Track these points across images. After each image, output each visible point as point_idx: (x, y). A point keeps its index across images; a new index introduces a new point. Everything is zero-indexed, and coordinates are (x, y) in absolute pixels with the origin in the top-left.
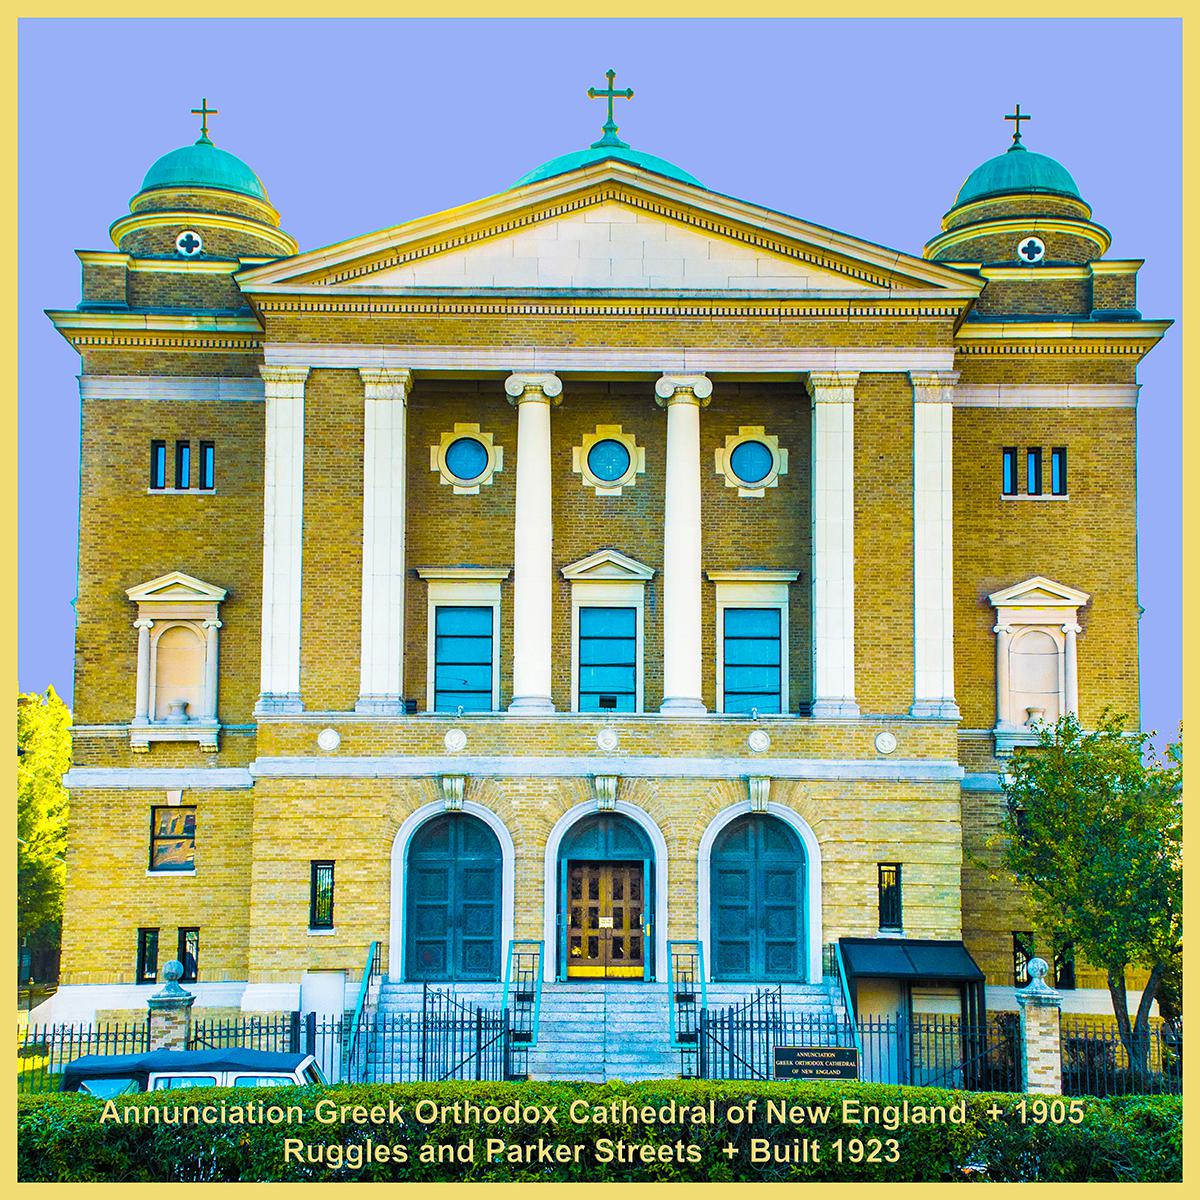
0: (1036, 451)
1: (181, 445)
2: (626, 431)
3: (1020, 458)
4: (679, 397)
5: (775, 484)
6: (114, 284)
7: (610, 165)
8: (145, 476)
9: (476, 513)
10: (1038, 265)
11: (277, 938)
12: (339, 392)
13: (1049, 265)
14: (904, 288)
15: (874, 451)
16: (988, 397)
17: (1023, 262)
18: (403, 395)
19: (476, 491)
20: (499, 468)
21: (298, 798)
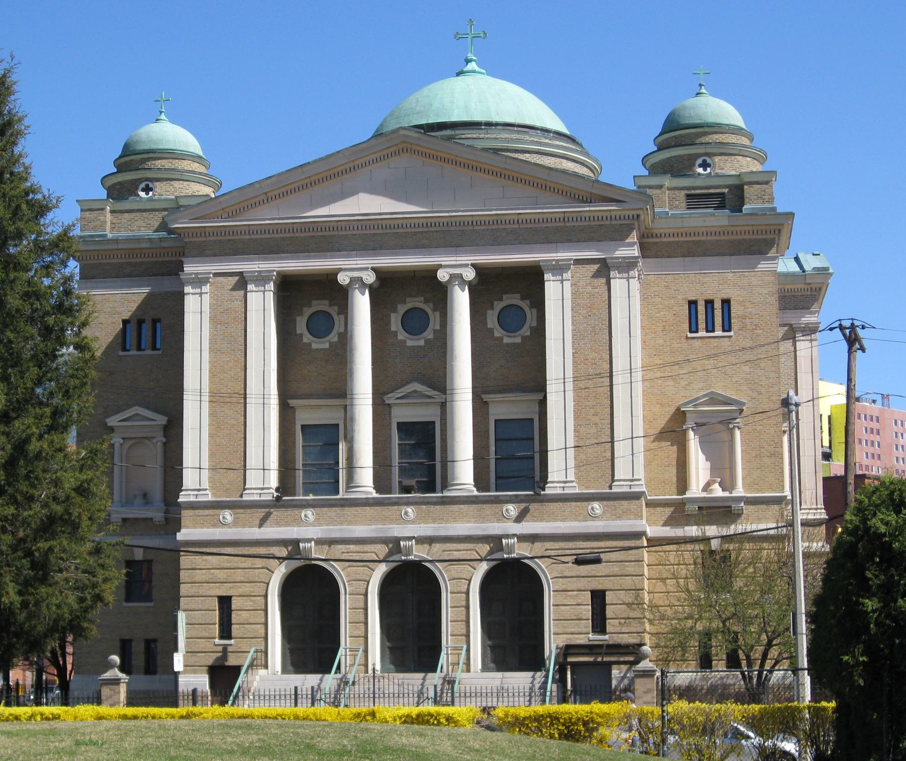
6: (99, 220)
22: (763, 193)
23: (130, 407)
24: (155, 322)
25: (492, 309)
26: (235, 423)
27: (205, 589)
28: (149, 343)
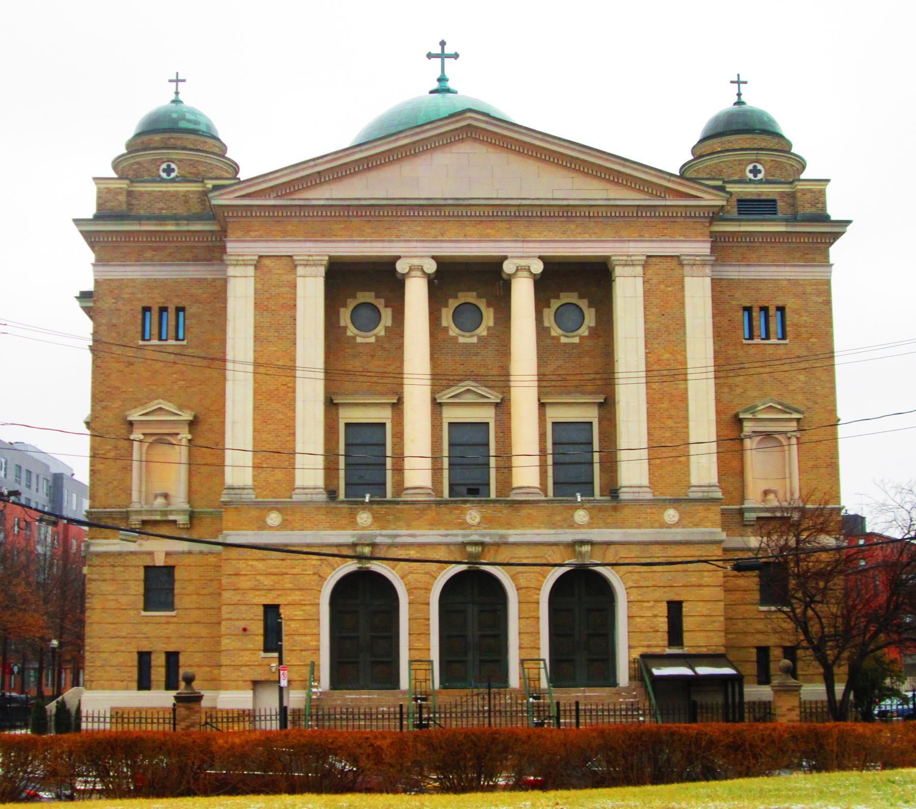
0: (765, 309)
1: (163, 310)
2: (377, 297)
3: (755, 314)
4: (413, 273)
5: (586, 334)
6: (117, 199)
7: (469, 115)
8: (137, 332)
9: (373, 356)
10: (760, 182)
11: (241, 659)
12: (279, 272)
13: (768, 182)
14: (671, 198)
15: (658, 310)
16: (732, 272)
17: (750, 180)
18: (323, 274)
19: (373, 340)
20: (389, 323)
21: (252, 560)
22: (816, 201)
25: (549, 307)
28: (172, 333)
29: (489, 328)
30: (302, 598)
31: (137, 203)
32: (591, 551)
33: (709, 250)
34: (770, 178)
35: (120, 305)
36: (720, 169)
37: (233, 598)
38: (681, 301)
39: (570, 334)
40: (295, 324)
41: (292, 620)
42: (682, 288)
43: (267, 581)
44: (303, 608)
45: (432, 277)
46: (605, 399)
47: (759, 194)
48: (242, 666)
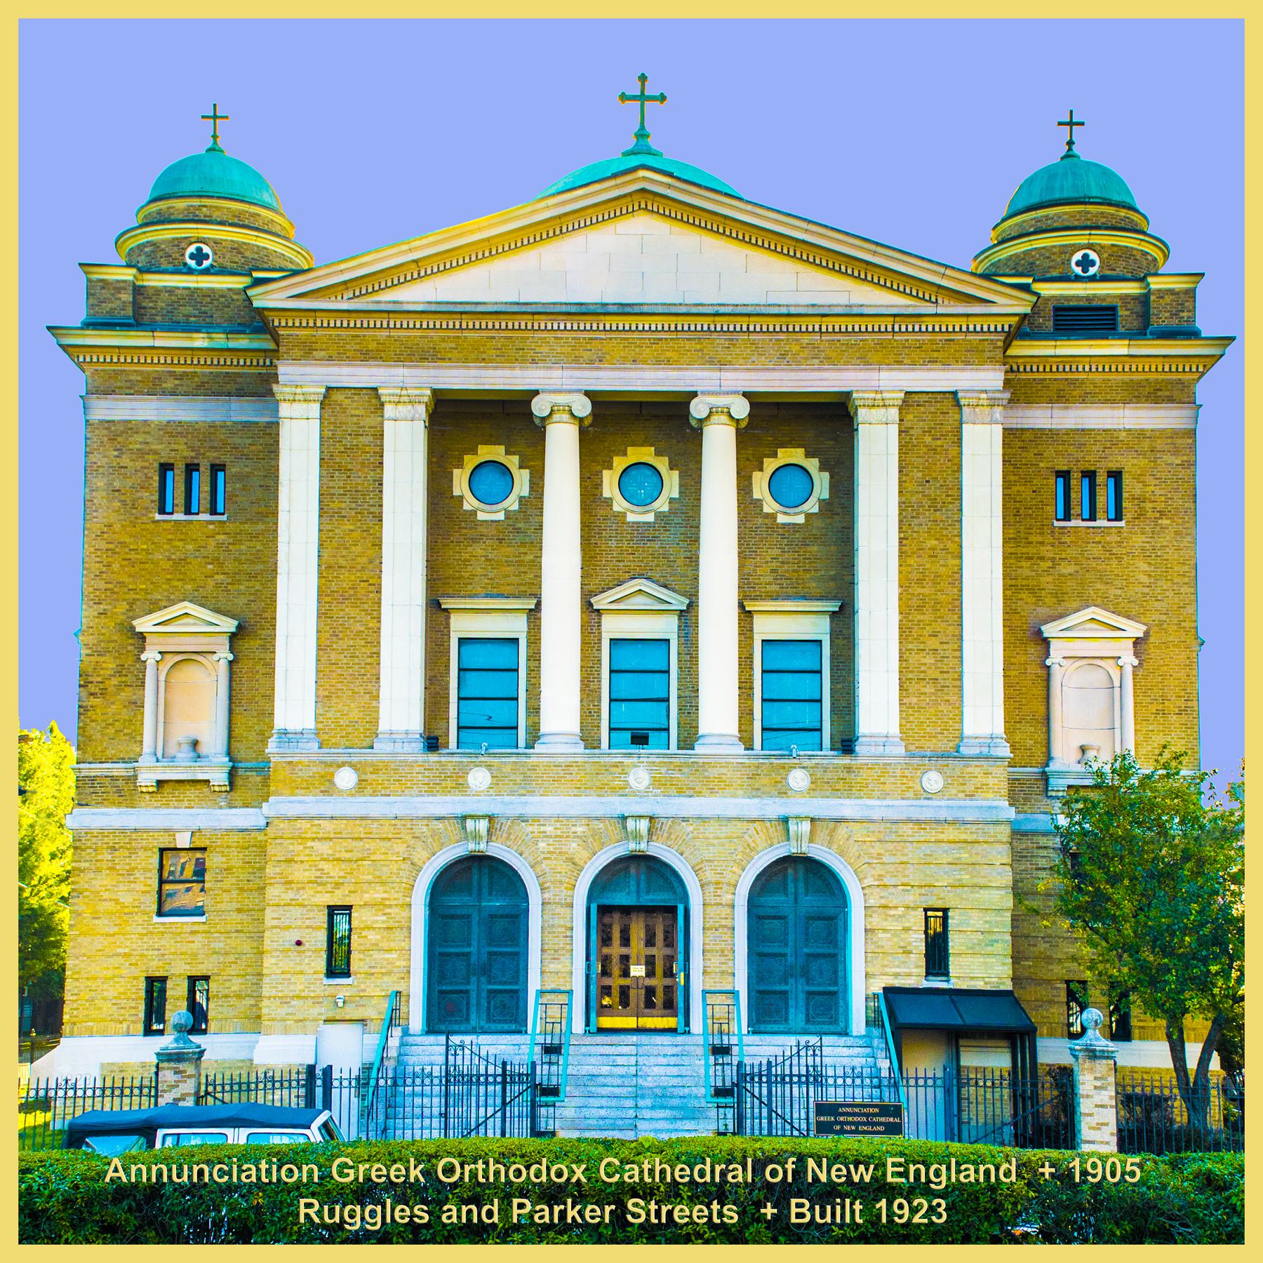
0: (1090, 475)
1: (191, 468)
3: (1073, 482)
4: (715, 418)
5: (816, 510)
6: (120, 299)
9: (500, 540)
10: (1092, 279)
11: (292, 987)
12: (357, 412)
13: (1104, 279)
14: (946, 302)
15: (920, 475)
16: (1040, 417)
18: (424, 416)
23: (173, 603)
24: (216, 468)
25: (761, 470)
26: (362, 629)
27: (307, 895)
28: (206, 504)
29: (672, 501)
30: (385, 896)
31: (151, 305)
32: (812, 832)
33: (1001, 383)
34: (1109, 273)
35: (125, 461)
36: (1031, 260)
37: (283, 896)
38: (956, 461)
39: (788, 510)
40: (381, 491)
41: (369, 928)
42: (959, 442)
43: (334, 871)
44: (387, 911)
45: (587, 423)
46: (841, 607)
47: (1088, 298)
48: (292, 998)
